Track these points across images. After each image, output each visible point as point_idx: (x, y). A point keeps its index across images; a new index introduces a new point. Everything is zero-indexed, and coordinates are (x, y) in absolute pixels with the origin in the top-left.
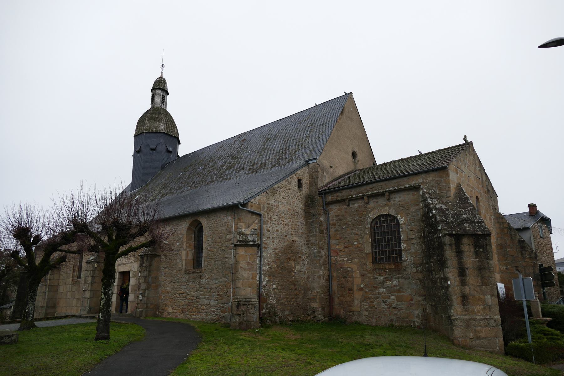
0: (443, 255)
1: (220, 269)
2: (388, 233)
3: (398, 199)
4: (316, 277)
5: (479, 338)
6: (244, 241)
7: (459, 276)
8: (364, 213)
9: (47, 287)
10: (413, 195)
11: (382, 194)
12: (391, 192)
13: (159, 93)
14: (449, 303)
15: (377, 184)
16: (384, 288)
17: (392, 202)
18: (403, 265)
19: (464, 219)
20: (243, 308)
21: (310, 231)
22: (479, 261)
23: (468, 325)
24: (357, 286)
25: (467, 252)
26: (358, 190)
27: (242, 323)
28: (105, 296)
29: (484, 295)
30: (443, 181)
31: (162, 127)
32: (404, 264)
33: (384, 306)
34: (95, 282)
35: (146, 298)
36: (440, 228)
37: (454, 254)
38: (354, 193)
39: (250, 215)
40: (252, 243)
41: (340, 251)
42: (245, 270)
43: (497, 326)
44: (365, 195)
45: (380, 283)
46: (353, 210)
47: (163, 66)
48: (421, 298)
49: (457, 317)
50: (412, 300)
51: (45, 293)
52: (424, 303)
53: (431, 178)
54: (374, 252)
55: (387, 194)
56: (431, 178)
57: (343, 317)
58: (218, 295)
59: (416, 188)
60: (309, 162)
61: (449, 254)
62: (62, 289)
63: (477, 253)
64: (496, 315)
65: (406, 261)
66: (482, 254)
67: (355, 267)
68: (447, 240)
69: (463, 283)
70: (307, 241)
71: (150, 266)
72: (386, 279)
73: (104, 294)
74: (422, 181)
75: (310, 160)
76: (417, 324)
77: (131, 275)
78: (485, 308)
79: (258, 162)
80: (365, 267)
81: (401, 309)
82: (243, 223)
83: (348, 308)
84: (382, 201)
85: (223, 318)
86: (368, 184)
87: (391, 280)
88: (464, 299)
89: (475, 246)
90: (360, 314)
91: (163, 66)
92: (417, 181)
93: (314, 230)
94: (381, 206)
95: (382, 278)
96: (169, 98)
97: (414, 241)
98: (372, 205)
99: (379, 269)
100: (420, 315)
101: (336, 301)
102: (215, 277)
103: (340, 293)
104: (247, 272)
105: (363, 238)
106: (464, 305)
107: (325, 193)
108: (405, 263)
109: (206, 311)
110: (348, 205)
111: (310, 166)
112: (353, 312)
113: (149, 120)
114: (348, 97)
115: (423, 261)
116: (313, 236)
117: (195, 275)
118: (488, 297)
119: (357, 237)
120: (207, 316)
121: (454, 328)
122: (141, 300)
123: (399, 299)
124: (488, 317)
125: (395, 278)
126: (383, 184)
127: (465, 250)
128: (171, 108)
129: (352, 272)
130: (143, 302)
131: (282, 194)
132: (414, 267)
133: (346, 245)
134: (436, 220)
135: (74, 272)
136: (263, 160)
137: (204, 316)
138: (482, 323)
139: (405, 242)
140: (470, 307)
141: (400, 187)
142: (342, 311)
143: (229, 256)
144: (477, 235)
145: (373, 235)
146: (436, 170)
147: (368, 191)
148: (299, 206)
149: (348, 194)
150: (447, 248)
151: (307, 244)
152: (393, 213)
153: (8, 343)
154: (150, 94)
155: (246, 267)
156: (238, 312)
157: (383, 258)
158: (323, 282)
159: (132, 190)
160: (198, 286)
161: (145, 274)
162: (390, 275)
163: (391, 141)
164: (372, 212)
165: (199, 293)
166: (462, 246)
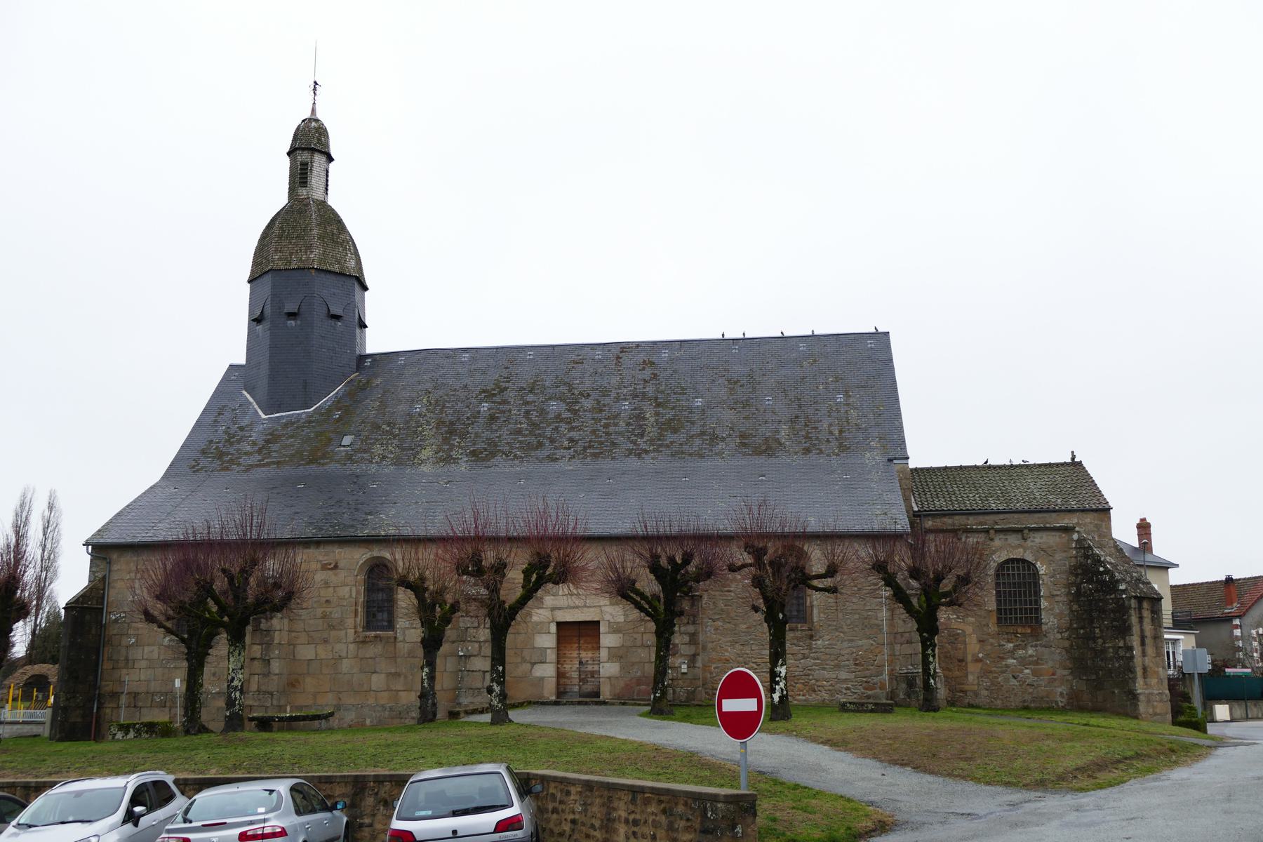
0: (1125, 621)
3: (1039, 539)
12: (1031, 530)
17: (1029, 543)
26: (981, 518)
33: (1014, 682)
38: (971, 521)
48: (1066, 672)
50: (1054, 674)
53: (1088, 518)
54: (999, 610)
59: (1067, 530)
61: (1134, 619)
63: (1153, 619)
69: (1144, 654)
72: (1017, 647)
77: (602, 629)
81: (1039, 686)
84: (1013, 539)
87: (1025, 648)
90: (976, 694)
97: (1058, 599)
112: (965, 692)
113: (322, 238)
114: (882, 338)
123: (1034, 673)
134: (1112, 577)
135: (356, 615)
139: (1046, 598)
146: (1097, 510)
150: (1132, 612)
152: (1029, 558)
160: (806, 652)
165: (809, 662)
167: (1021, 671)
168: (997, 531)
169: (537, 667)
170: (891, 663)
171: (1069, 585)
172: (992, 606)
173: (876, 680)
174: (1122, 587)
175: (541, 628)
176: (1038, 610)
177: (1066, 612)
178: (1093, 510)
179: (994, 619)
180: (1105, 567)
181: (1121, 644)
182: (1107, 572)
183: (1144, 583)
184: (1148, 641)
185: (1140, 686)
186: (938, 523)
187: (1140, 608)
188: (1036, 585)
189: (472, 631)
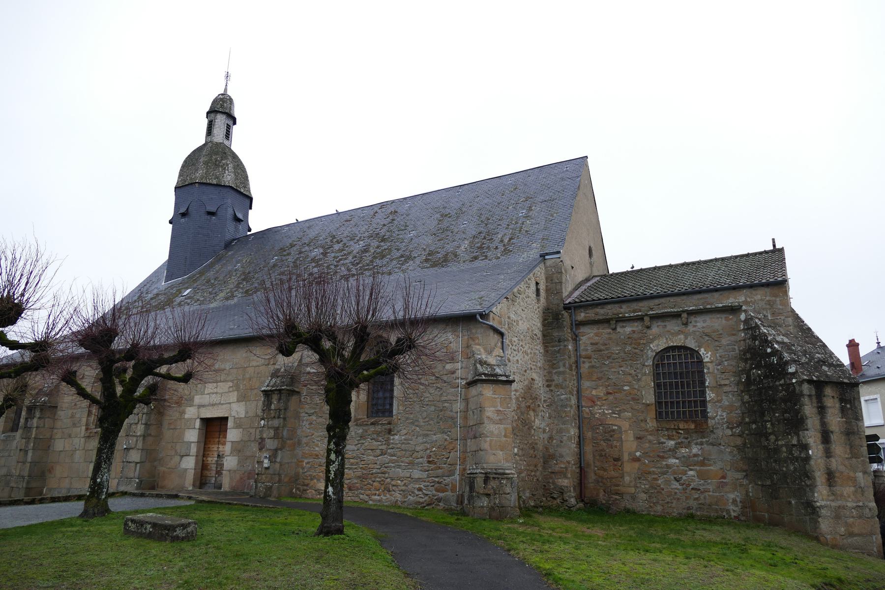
0: (798, 412)
1: (432, 419)
2: (681, 373)
3: (701, 323)
4: (565, 438)
5: (852, 535)
6: (492, 375)
7: (823, 443)
8: (642, 342)
9: (32, 440)
10: (727, 319)
11: (677, 315)
12: (691, 313)
13: (221, 120)
14: (808, 483)
15: (668, 299)
16: (677, 459)
17: (691, 328)
18: (710, 425)
19: (820, 360)
20: (493, 484)
21: (553, 366)
22: (846, 422)
23: (837, 516)
24: (630, 454)
25: (830, 407)
26: (635, 306)
27: (492, 509)
28: (337, 457)
29: (855, 472)
30: (778, 302)
31: (229, 178)
32: (711, 422)
33: (676, 485)
34: (150, 435)
35: (277, 466)
36: (790, 370)
37: (815, 410)
38: (625, 310)
39: (491, 333)
40: (504, 378)
41: (599, 398)
42: (495, 423)
43: (872, 517)
44: (647, 315)
45: (670, 450)
46: (622, 337)
47: (227, 76)
48: (739, 475)
49: (823, 503)
50: (724, 477)
51: (26, 452)
52: (745, 482)
53: (759, 296)
54: (659, 403)
55: (684, 315)
56: (759, 297)
57: (604, 502)
58: (429, 462)
59: (734, 310)
60: (547, 257)
61: (809, 409)
62: (59, 445)
63: (843, 410)
64: (870, 501)
65: (714, 418)
66: (850, 412)
67: (625, 425)
68: (806, 388)
69: (828, 454)
70: (547, 381)
71: (285, 409)
72: (679, 445)
73: (336, 452)
74: (743, 299)
75: (547, 254)
76: (733, 514)
77: (230, 424)
78: (856, 491)
79: (439, 250)
80: (643, 424)
82: (479, 345)
83: (613, 488)
84: (673, 326)
85: (439, 500)
86: (652, 297)
87: (688, 446)
88: (830, 476)
89: (841, 400)
90: (634, 497)
91: (227, 76)
92: (735, 298)
93: (561, 364)
94: (672, 334)
95: (672, 443)
96: (235, 129)
97: (726, 389)
98: (655, 329)
99: (667, 429)
100: (738, 500)
101: (591, 477)
102: (421, 432)
103: (598, 464)
104: (497, 426)
105: (639, 380)
106: (830, 486)
107: (575, 308)
108: (713, 421)
109: (403, 488)
110: (615, 329)
111: (548, 263)
113: (206, 163)
114: (775, 256)
115: (743, 419)
116: (559, 373)
117: (378, 428)
118: (860, 475)
119: (630, 378)
120: (405, 496)
121: (820, 519)
122: (267, 468)
123: (701, 475)
124: (861, 504)
125: (696, 444)
126: (678, 299)
127: (829, 405)
128: (239, 144)
129: (621, 433)
130: (271, 471)
131: (522, 303)
132: (728, 428)
133: (610, 390)
134: (781, 358)
136: (450, 248)
137: (398, 496)
138: (854, 512)
139: (712, 389)
140: (838, 489)
141: (709, 306)
142: (602, 493)
143: (450, 397)
144: (842, 383)
145: (656, 376)
146: (768, 285)
147: (652, 309)
148: (537, 324)
149: (615, 312)
150: (806, 400)
151: (548, 386)
152: (691, 344)
153: (183, 539)
154: (205, 122)
155: (495, 417)
156: (486, 491)
157: (672, 412)
158: (573, 446)
159: (168, 279)
160: (384, 447)
161: (276, 423)
162: (687, 438)
163: (639, 234)
164: (656, 342)
165: (386, 458)
166: (825, 399)
167: (685, 473)
168: (654, 318)
169: (185, 459)
170: (463, 461)
171: (738, 374)
172: (649, 397)
173: (448, 480)
174: (792, 369)
175: (189, 425)
176: (704, 403)
177: (738, 404)
178: (762, 285)
179: (653, 414)
180: (772, 347)
181: (795, 442)
182: (775, 352)
183: (830, 365)
184: (837, 438)
185: (821, 495)
186: (591, 314)
187: (819, 396)
188: (701, 374)
189: (133, 426)
